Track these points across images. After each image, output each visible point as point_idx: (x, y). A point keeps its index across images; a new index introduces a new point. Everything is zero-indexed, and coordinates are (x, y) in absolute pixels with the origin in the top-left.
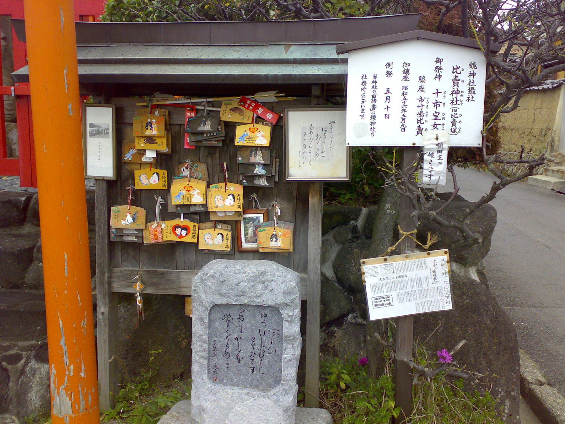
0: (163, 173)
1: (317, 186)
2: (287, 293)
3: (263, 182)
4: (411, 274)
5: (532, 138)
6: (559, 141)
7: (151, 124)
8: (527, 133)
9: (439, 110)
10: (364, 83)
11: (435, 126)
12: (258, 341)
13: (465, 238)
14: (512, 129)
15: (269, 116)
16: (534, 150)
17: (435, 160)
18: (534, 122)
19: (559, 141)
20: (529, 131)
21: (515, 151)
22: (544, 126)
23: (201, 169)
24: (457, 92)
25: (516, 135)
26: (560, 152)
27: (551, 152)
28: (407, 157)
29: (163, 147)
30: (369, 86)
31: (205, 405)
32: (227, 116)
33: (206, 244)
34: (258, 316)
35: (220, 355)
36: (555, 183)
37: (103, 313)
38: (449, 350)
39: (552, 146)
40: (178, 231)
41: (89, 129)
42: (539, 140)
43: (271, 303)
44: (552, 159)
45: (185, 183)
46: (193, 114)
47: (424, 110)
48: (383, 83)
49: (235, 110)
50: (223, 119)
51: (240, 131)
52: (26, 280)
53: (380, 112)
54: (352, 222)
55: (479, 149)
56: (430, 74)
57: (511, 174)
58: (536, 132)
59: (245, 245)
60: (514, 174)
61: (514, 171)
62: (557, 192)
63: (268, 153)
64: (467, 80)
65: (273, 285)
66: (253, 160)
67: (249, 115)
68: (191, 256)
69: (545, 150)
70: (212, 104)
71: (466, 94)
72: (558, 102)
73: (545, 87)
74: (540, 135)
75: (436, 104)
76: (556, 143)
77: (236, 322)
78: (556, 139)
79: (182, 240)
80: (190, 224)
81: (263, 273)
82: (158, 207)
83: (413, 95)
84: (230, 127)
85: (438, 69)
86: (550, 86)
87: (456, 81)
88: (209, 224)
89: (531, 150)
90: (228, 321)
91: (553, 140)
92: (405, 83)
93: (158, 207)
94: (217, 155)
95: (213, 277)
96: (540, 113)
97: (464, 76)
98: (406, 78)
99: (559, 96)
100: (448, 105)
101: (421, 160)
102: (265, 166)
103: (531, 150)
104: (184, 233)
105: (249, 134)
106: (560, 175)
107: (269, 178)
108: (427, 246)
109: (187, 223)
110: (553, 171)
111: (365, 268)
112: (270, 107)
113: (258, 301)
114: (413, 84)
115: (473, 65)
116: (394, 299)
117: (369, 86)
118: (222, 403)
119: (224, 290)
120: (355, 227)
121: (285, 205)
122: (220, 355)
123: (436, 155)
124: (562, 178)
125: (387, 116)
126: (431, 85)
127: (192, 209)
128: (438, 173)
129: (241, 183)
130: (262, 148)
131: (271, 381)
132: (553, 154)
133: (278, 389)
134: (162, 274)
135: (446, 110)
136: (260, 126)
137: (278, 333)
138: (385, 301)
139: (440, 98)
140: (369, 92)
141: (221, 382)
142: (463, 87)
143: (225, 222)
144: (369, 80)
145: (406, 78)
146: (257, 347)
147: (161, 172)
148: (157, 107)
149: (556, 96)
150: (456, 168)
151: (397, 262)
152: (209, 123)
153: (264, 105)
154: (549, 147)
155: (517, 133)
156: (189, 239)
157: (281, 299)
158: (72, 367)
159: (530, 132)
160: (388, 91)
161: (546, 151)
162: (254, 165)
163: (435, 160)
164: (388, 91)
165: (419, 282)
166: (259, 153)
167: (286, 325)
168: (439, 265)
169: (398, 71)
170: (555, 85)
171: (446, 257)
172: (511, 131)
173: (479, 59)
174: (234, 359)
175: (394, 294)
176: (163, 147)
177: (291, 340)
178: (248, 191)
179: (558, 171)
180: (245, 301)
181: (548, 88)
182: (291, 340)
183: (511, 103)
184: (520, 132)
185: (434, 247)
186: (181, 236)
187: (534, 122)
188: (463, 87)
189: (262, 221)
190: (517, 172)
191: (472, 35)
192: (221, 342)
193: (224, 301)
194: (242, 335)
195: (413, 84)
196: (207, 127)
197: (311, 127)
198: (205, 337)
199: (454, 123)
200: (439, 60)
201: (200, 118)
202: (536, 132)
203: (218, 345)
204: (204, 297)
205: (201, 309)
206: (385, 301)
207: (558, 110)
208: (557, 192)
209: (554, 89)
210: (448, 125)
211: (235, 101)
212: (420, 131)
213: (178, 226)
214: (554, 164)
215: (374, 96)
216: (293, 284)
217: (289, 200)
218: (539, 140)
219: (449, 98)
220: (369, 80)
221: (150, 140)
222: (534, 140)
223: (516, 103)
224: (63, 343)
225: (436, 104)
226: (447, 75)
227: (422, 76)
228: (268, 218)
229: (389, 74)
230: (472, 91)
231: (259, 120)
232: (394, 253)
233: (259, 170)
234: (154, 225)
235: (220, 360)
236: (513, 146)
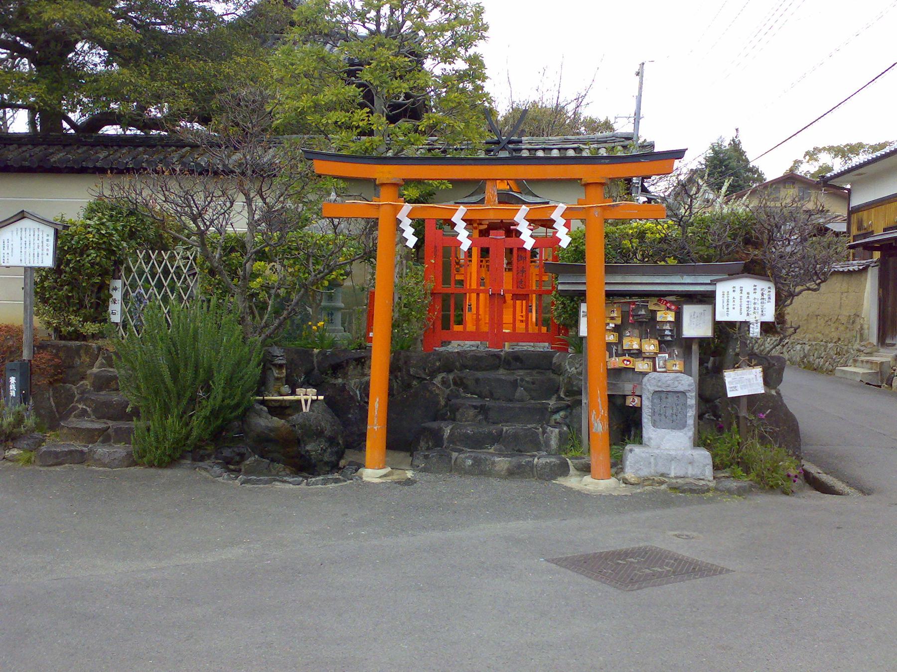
0: (616, 334)
1: (696, 340)
2: (689, 385)
3: (669, 338)
4: (745, 377)
5: (840, 325)
6: (868, 329)
7: (614, 311)
8: (834, 320)
9: (756, 306)
10: (724, 294)
11: (754, 313)
12: (675, 408)
13: (769, 364)
14: (817, 316)
15: (673, 307)
16: (842, 339)
17: (755, 327)
18: (840, 308)
19: (868, 329)
20: (836, 317)
21: (822, 341)
22: (853, 312)
23: (636, 332)
24: (763, 299)
25: (822, 322)
26: (870, 341)
27: (861, 340)
28: (743, 325)
29: (619, 322)
30: (726, 296)
31: (651, 436)
32: (651, 307)
33: (639, 369)
34: (675, 397)
35: (657, 415)
36: (864, 373)
37: (585, 403)
38: (763, 414)
39: (862, 335)
40: (625, 362)
41: (582, 314)
42: (847, 328)
43: (682, 390)
44: (862, 348)
45: (630, 339)
46: (634, 306)
47: (749, 306)
48: (732, 295)
49: (656, 304)
50: (650, 309)
51: (659, 314)
52: (515, 397)
53: (731, 307)
54: (706, 364)
55: (773, 323)
56: (751, 292)
57: (818, 367)
58: (844, 320)
59: (658, 370)
60: (821, 367)
61: (821, 364)
62: (867, 384)
63: (672, 325)
64: (767, 294)
65: (683, 382)
66: (664, 328)
67: (663, 307)
68: (630, 375)
69: (854, 339)
70: (643, 302)
71: (767, 300)
72: (865, 286)
73: (851, 268)
74: (848, 322)
75: (755, 303)
76: (866, 331)
77: (664, 400)
78: (866, 326)
79: (628, 366)
80: (631, 359)
81: (678, 377)
82: (614, 351)
83: (745, 300)
84: (654, 312)
85: (755, 289)
86: (856, 268)
87: (762, 295)
88: (641, 359)
89: (839, 339)
90: (661, 399)
91: (862, 328)
92: (741, 295)
93: (614, 351)
94: (644, 325)
95: (654, 378)
96: (846, 297)
97: (766, 292)
98: (741, 293)
99: (866, 279)
100: (760, 304)
101: (749, 327)
102: (670, 330)
103: (839, 339)
104: (628, 363)
105: (664, 315)
106: (869, 365)
107: (672, 336)
108: (752, 365)
109: (629, 358)
110: (862, 361)
111: (725, 374)
112: (672, 303)
113: (676, 389)
114: (745, 295)
115: (769, 288)
116: (739, 388)
117: (726, 296)
118: (659, 435)
119: (659, 384)
120: (707, 367)
121: (679, 350)
122: (657, 415)
123: (755, 325)
124: (872, 369)
125: (734, 308)
126: (752, 296)
127: (632, 352)
128: (757, 333)
129: (657, 339)
130: (669, 322)
131: (681, 427)
132: (862, 343)
133: (686, 429)
134: (614, 384)
135: (759, 306)
136: (668, 312)
137: (685, 404)
138: (734, 389)
139: (756, 301)
140: (726, 298)
141: (657, 427)
142: (766, 297)
143: (648, 358)
144: (726, 294)
145: (741, 293)
146: (674, 411)
147: (615, 334)
148: (615, 303)
149: (863, 279)
150: (830, 166)
151: (739, 372)
152: (643, 310)
153: (670, 302)
154: (858, 336)
155: (822, 320)
156: (631, 366)
157: (686, 388)
158: (603, 411)
159: (837, 319)
160: (734, 298)
161: (856, 341)
162: (665, 330)
163: (755, 327)
164: (734, 298)
165: (749, 380)
166: (668, 324)
167: (688, 400)
168: (758, 373)
169: (738, 290)
170: (861, 267)
171: (761, 369)
172: (816, 318)
173: (772, 285)
174: (663, 417)
175: (738, 385)
176: (619, 322)
177: (691, 407)
178: (660, 343)
179: (867, 362)
180: (669, 389)
181: (854, 270)
182: (691, 407)
183: (789, 302)
184: (826, 319)
185: (756, 365)
186: (627, 365)
187: (840, 308)
188: (766, 297)
189: (667, 357)
190: (824, 364)
191: (769, 276)
192: (657, 409)
193: (660, 389)
194: (667, 406)
195: (745, 295)
196: (643, 312)
197: (695, 312)
198: (650, 406)
199: (762, 311)
200: (755, 286)
201: (639, 308)
202: (844, 320)
203: (656, 411)
204: (649, 387)
205: (647, 393)
206: (734, 389)
207: (866, 294)
208: (867, 384)
209: (860, 271)
210: (760, 312)
211: (655, 300)
212: (748, 315)
213: (625, 360)
214: (864, 355)
215: (728, 300)
216: (693, 381)
217: (681, 347)
218: (847, 328)
219: (760, 301)
220: (726, 294)
221: (612, 318)
222: (842, 328)
223: (792, 301)
224: (599, 400)
225: (755, 303)
226: (759, 292)
227: (485, 34)
228: (670, 356)
229: (734, 291)
230: (769, 298)
231: (668, 309)
232: (738, 367)
233: (667, 333)
234: (613, 359)
235: (657, 417)
236: (819, 335)
